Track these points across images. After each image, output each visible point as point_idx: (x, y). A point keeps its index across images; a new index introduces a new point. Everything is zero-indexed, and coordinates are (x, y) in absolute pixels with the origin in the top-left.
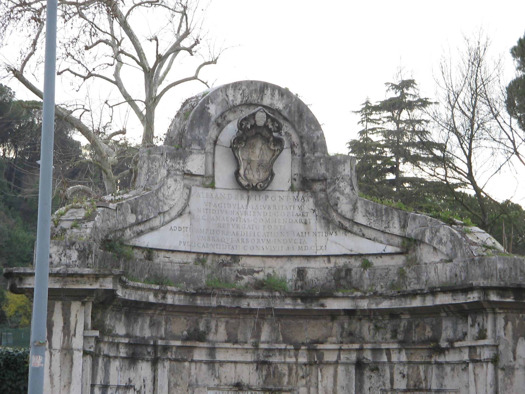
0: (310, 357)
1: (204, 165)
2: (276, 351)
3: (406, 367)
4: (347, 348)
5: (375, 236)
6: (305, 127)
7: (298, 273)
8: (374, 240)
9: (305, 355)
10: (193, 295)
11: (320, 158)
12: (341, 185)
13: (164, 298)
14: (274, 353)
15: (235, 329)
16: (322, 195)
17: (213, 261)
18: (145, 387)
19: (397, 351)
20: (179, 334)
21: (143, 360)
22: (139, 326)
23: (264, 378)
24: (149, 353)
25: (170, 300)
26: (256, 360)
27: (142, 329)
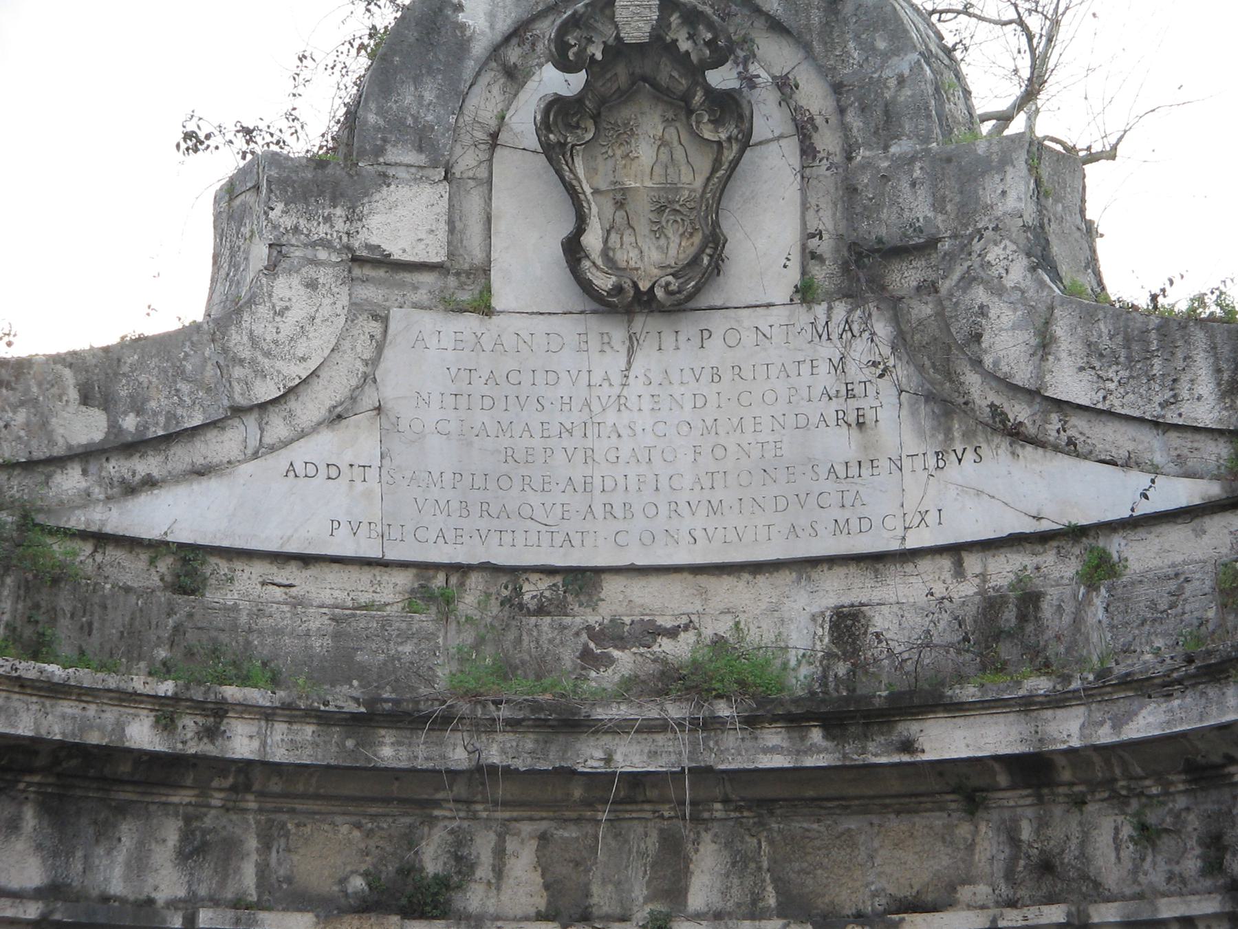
1: (443, 227)
5: (1131, 446)
6: (851, 45)
7: (835, 626)
8: (1128, 463)
10: (353, 722)
11: (912, 160)
12: (994, 254)
13: (211, 733)
15: (577, 864)
16: (923, 310)
17: (488, 595)
20: (330, 888)
22: (121, 856)
25: (242, 742)
27: (139, 865)
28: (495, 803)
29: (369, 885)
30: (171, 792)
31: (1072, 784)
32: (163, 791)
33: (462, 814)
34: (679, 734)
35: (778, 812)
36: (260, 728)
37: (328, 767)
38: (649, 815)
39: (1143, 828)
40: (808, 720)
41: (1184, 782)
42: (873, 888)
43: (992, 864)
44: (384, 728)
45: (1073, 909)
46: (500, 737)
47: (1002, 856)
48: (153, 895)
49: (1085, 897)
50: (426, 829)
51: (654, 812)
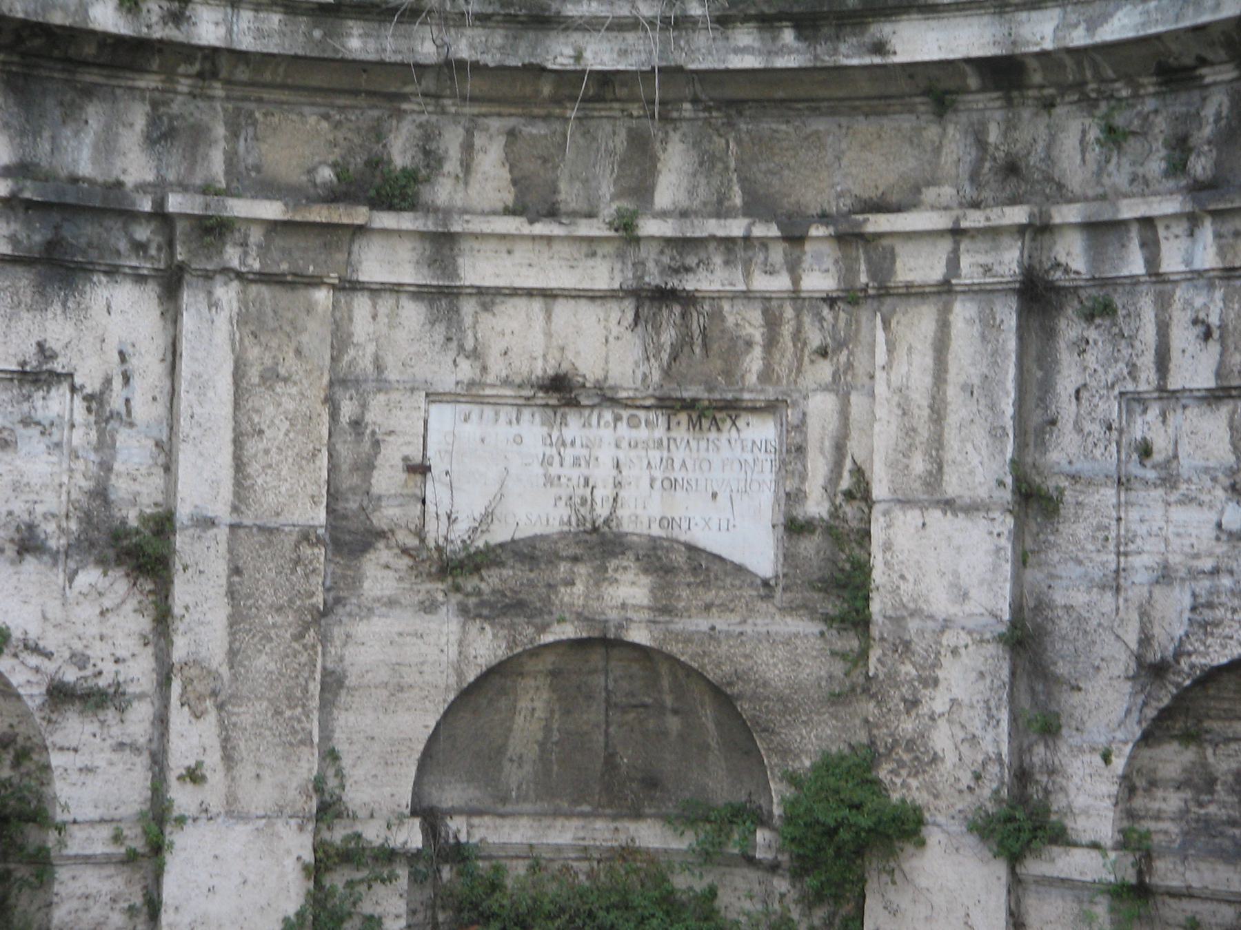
0: (848, 272)
2: (712, 246)
3: (1218, 294)
4: (982, 223)
9: (828, 263)
14: (703, 255)
15: (545, 161)
18: (127, 379)
19: (1180, 228)
21: (112, 272)
22: (88, 138)
23: (665, 356)
24: (139, 247)
26: (631, 284)
27: (107, 147)
28: (464, 98)
29: (337, 175)
30: (137, 76)
31: (1042, 87)
32: (129, 75)
33: (430, 109)
34: (649, 32)
35: (747, 113)
36: (226, 14)
37: (296, 57)
38: (618, 114)
39: (1110, 130)
40: (780, 20)
41: (1154, 84)
42: (839, 189)
43: (957, 167)
44: (351, 19)
45: (1036, 210)
46: (468, 32)
47: (968, 158)
48: (122, 178)
49: (1048, 198)
50: (394, 122)
51: (623, 111)
